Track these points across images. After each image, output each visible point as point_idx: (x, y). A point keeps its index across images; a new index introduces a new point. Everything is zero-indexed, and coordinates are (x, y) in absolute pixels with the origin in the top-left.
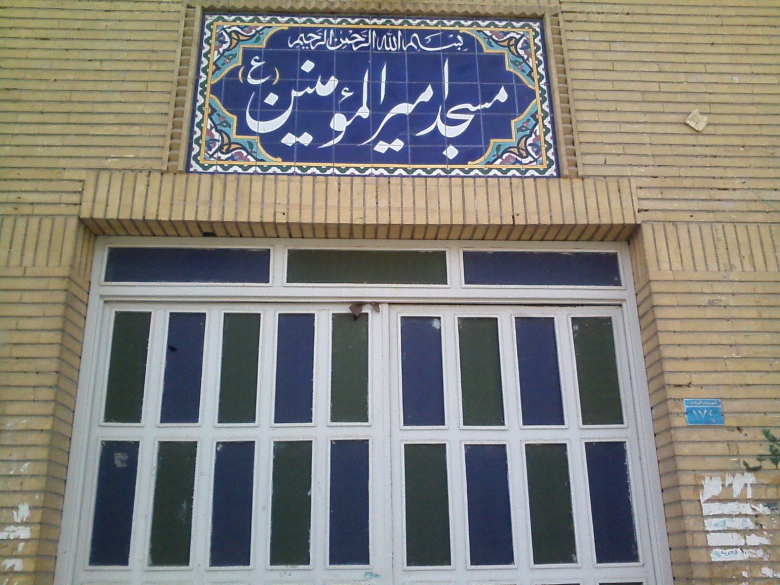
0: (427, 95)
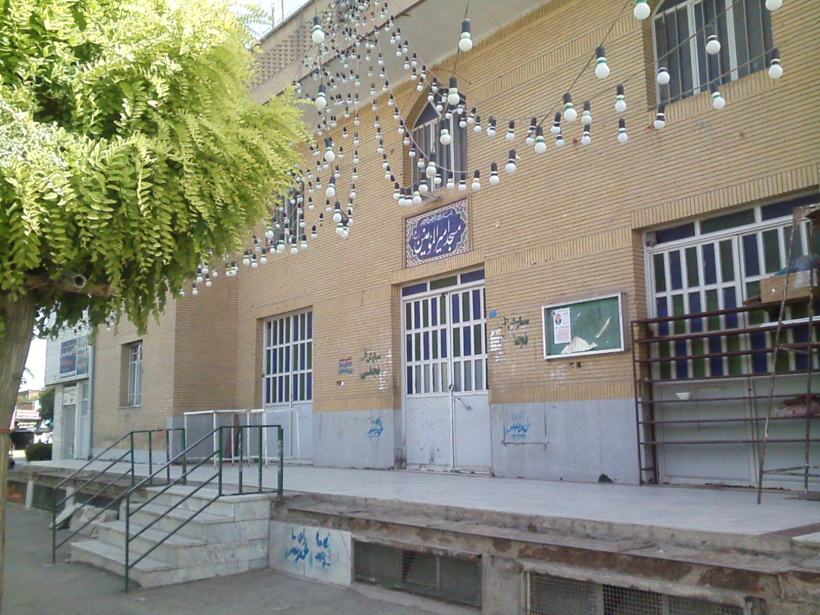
0: (445, 233)
